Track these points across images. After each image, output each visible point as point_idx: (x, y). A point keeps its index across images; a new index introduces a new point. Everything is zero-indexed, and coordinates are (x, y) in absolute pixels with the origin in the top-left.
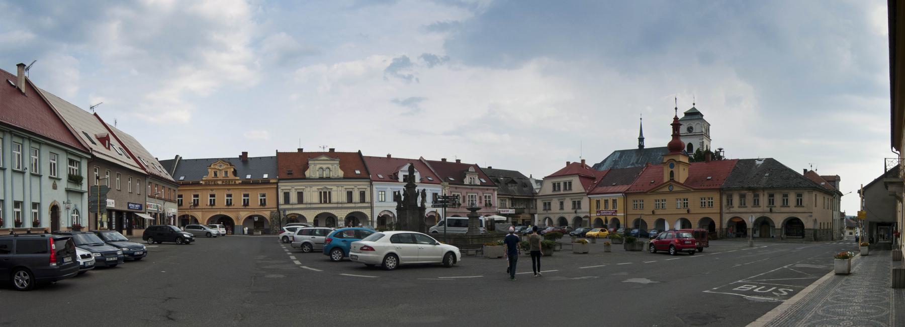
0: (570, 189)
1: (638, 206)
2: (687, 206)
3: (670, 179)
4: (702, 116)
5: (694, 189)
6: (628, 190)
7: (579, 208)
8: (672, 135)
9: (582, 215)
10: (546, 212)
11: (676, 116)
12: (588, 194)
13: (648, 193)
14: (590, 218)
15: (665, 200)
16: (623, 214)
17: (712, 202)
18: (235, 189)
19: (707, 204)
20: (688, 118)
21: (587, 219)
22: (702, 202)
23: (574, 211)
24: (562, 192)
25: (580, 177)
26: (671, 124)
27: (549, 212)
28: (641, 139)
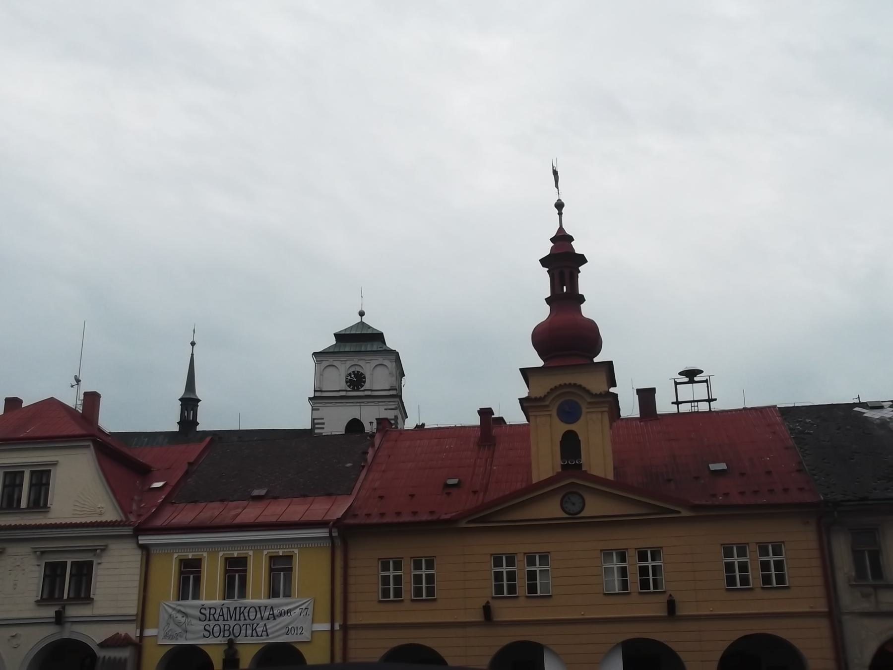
0: (39, 502)
3: (563, 467)
5: (694, 507)
7: (83, 595)
8: (548, 300)
9: (95, 635)
11: (561, 229)
12: (140, 530)
13: (463, 524)
14: (138, 646)
15: (544, 558)
16: (326, 627)
17: (779, 565)
18: (51, 604)
21: (125, 654)
22: (386, 580)
23: (50, 612)
25: (95, 442)
28: (189, 403)
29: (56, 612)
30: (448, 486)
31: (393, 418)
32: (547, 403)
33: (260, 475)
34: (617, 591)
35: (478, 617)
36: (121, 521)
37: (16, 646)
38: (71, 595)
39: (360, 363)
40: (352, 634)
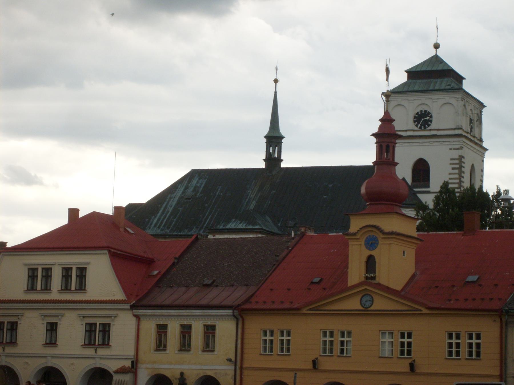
0: (81, 287)
1: (277, 346)
2: (409, 353)
3: (367, 278)
4: (459, 79)
6: (248, 300)
7: (106, 343)
9: (112, 366)
10: (90, 351)
13: (304, 311)
17: (478, 346)
19: (464, 350)
20: (419, 84)
24: (55, 294)
25: (109, 251)
26: (373, 135)
27: (102, 352)
29: (375, 280)
30: (313, 283)
31: (457, 157)
32: (358, 237)
33: (215, 268)
34: (387, 356)
35: (310, 366)
36: (125, 300)
37: (73, 370)
38: (100, 343)
39: (427, 102)
40: (246, 373)
